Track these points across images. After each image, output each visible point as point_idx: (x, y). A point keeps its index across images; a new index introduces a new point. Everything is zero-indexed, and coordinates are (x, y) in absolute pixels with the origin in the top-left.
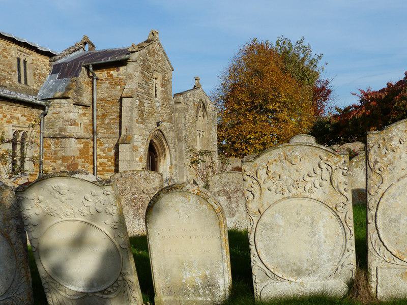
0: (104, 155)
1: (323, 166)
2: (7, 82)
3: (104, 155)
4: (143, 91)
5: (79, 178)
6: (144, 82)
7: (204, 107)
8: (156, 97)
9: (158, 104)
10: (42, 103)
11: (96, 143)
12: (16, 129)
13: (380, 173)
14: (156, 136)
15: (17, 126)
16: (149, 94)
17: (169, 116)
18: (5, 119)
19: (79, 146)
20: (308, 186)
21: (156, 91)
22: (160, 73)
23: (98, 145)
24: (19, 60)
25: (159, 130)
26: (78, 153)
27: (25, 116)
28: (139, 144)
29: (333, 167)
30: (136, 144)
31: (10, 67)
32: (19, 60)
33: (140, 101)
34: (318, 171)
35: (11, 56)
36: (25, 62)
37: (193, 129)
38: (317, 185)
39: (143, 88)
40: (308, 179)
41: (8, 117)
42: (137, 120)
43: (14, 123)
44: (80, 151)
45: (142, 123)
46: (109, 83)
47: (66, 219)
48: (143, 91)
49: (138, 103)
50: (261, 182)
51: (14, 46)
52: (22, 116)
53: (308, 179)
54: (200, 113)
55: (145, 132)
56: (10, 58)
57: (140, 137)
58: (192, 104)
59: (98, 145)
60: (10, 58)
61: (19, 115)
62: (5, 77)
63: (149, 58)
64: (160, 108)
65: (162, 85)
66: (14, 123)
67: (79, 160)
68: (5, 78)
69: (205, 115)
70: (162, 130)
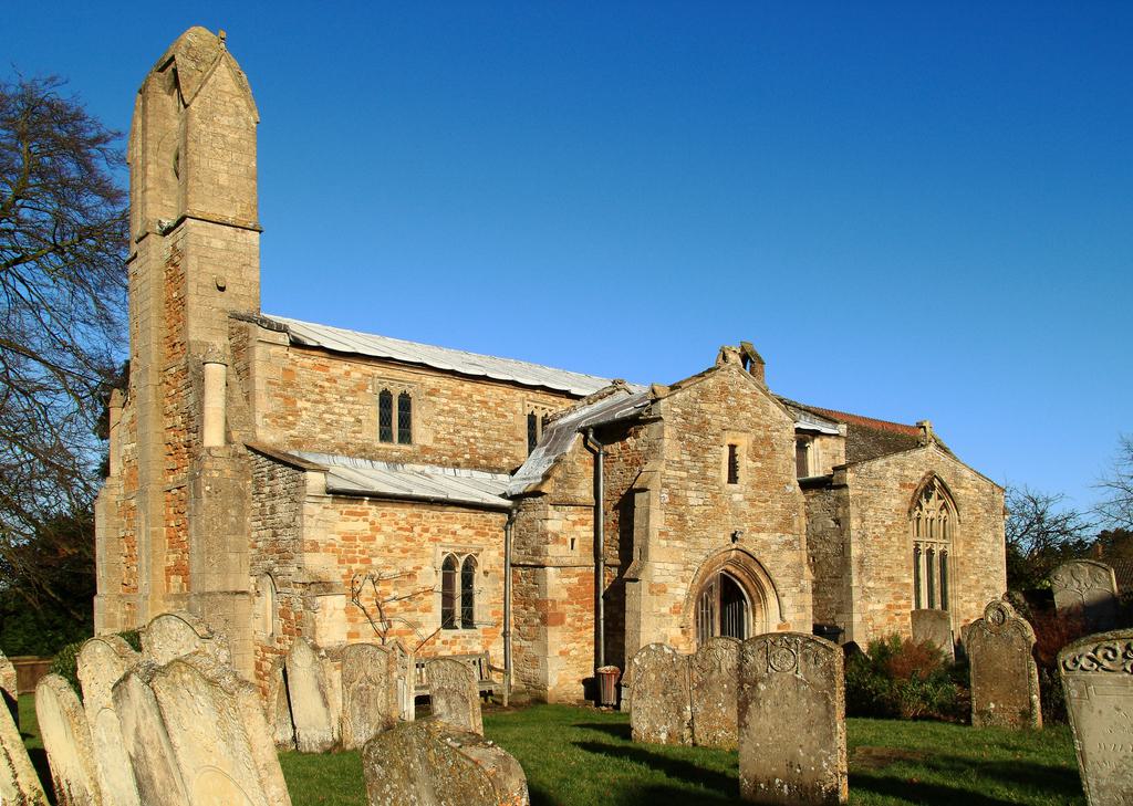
2: (505, 460)
4: (684, 474)
11: (605, 575)
12: (450, 551)
15: (451, 547)
19: (566, 581)
23: (607, 579)
26: (564, 595)
27: (472, 528)
30: (657, 580)
35: (515, 413)
43: (446, 540)
44: (569, 589)
48: (684, 474)
51: (520, 394)
52: (463, 528)
56: (510, 416)
59: (607, 579)
60: (510, 416)
61: (457, 527)
62: (500, 451)
63: (704, 406)
64: (745, 506)
66: (446, 540)
67: (568, 607)
68: (501, 453)
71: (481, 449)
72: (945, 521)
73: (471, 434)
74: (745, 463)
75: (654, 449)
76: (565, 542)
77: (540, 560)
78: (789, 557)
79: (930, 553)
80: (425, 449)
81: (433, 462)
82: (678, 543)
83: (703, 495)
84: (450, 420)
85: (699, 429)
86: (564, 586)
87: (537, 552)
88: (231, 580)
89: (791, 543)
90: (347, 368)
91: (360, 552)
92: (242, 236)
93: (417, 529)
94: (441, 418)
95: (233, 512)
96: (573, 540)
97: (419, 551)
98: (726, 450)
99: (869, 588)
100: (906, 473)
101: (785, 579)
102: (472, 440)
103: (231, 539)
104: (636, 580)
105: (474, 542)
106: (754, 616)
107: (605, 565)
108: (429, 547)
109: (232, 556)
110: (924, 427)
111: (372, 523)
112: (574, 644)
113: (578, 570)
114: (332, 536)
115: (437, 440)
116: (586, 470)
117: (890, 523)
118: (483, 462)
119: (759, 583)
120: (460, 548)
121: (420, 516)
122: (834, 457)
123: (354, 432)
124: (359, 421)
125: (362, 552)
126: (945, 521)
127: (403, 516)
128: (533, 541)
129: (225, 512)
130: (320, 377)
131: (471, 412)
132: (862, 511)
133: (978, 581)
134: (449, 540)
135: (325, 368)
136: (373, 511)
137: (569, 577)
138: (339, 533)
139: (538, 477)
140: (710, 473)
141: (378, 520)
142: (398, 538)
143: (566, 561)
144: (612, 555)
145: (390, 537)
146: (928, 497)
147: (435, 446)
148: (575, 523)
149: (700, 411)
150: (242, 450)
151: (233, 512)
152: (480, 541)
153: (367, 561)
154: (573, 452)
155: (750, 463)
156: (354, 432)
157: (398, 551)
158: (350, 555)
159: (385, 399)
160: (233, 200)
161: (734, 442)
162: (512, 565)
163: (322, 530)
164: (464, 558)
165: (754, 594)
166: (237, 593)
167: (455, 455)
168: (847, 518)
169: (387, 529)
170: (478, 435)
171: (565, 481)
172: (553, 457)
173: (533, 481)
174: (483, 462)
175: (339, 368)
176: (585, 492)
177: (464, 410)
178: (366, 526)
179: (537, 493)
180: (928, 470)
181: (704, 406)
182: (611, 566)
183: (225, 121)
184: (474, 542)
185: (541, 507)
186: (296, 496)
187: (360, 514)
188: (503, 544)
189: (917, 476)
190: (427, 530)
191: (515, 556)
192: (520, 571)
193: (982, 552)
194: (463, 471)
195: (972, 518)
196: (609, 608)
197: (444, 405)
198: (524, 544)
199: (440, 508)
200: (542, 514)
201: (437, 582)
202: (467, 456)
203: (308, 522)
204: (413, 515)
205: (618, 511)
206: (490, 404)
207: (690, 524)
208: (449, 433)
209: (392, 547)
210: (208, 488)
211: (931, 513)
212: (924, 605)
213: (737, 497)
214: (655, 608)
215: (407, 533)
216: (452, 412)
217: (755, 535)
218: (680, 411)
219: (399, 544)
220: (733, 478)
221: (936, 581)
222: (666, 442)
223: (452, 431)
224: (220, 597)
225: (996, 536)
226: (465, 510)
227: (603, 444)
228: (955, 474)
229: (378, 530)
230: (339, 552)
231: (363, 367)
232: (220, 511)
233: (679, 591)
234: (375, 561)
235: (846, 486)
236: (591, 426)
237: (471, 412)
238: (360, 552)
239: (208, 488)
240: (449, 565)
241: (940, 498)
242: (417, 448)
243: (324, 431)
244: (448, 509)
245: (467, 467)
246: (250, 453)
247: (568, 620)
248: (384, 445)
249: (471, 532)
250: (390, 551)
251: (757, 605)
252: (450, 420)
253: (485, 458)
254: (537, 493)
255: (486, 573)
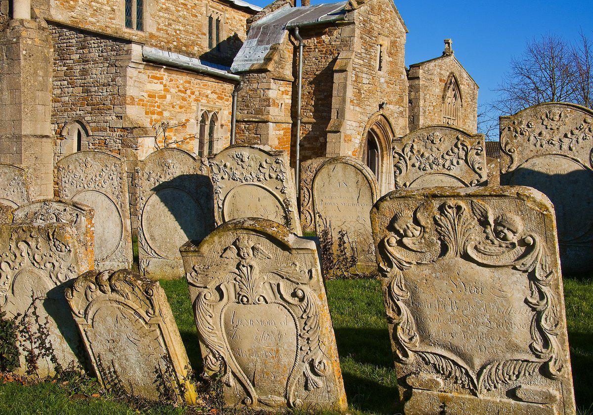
0: (308, 146)
1: (460, 146)
3: (308, 146)
4: (362, 62)
5: (257, 148)
6: (363, 51)
7: (457, 84)
8: (380, 69)
9: (382, 80)
10: (237, 77)
12: (205, 109)
13: (510, 153)
14: (378, 124)
16: (370, 66)
17: (397, 97)
18: (193, 97)
19: (278, 132)
20: (447, 164)
21: (380, 62)
22: (387, 37)
24: (211, 18)
25: (382, 115)
27: (216, 93)
28: (354, 132)
29: (469, 147)
30: (348, 132)
31: (200, 28)
32: (211, 18)
33: (357, 76)
34: (456, 150)
36: (218, 21)
37: (436, 115)
38: (455, 163)
39: (361, 58)
40: (447, 157)
41: (197, 93)
42: (352, 101)
44: (279, 139)
45: (358, 105)
46: (319, 51)
47: (246, 183)
48: (362, 62)
49: (354, 79)
50: (407, 159)
52: (212, 93)
53: (447, 157)
54: (450, 93)
55: (362, 117)
57: (354, 124)
58: (437, 79)
59: (301, 132)
63: (372, 17)
64: (385, 85)
65: (390, 54)
68: (194, 43)
69: (458, 95)
70: (387, 115)
73: (177, 27)
74: (386, 58)
75: (346, 44)
77: (264, 117)
80: (152, 36)
81: (156, 46)
82: (357, 108)
87: (259, 112)
88: (39, 126)
93: (188, 92)
94: (161, 14)
95: (40, 73)
96: (282, 104)
102: (178, 32)
103: (39, 94)
104: (339, 132)
105: (217, 103)
106: (382, 160)
107: (301, 123)
108: (194, 106)
109: (40, 108)
110: (449, 43)
111: (165, 86)
114: (143, 94)
115: (159, 30)
116: (289, 56)
118: (184, 48)
120: (210, 107)
121: (189, 82)
123: (110, 18)
124: (113, 10)
125: (159, 107)
127: (181, 82)
128: (256, 104)
129: (35, 73)
131: (178, 11)
134: (204, 101)
137: (279, 130)
138: (147, 92)
139: (260, 60)
141: (168, 84)
144: (307, 116)
147: (157, 34)
150: (44, 24)
151: (40, 73)
152: (219, 104)
153: (160, 113)
154: (283, 43)
156: (110, 18)
157: (177, 107)
158: (152, 108)
162: (237, 121)
163: (137, 89)
165: (384, 145)
166: (43, 137)
167: (168, 42)
168: (418, 99)
169: (173, 91)
171: (280, 63)
172: (269, 46)
173: (255, 62)
174: (184, 48)
176: (288, 72)
177: (174, 9)
178: (161, 87)
179: (262, 70)
180: (450, 71)
181: (372, 17)
182: (305, 123)
184: (217, 103)
185: (264, 80)
186: (117, 66)
188: (231, 106)
190: (193, 93)
191: (239, 115)
192: (243, 126)
194: (173, 54)
196: (303, 152)
198: (247, 106)
199: (201, 77)
200: (265, 86)
201: (196, 130)
202: (175, 43)
203: (130, 82)
205: (313, 86)
208: (165, 26)
209: (175, 104)
210: (24, 52)
215: (183, 95)
219: (178, 102)
222: (356, 39)
223: (167, 24)
224: (32, 139)
226: (214, 80)
227: (303, 39)
228: (460, 75)
230: (146, 105)
232: (32, 71)
234: (166, 114)
235: (418, 78)
236: (298, 26)
237: (178, 11)
239: (24, 52)
240: (204, 117)
243: (93, 15)
245: (175, 52)
246: (51, 27)
248: (128, 30)
249: (215, 96)
250: (173, 107)
251: (385, 152)
252: (166, 15)
253: (185, 46)
254: (262, 70)
255: (222, 126)
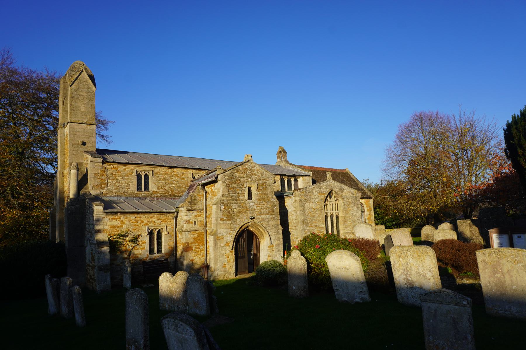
4: (230, 198)
56: (186, 179)
63: (238, 175)
64: (254, 207)
67: (193, 244)
71: (175, 190)
72: (337, 205)
73: (171, 186)
76: (192, 223)
78: (272, 222)
79: (332, 216)
82: (228, 222)
83: (237, 205)
84: (164, 182)
85: (235, 183)
86: (191, 238)
89: (274, 218)
90: (125, 168)
91: (117, 231)
92: (89, 127)
93: (139, 222)
94: (160, 181)
96: (195, 222)
97: (140, 229)
98: (247, 189)
99: (307, 230)
100: (321, 190)
101: (272, 230)
112: (196, 257)
113: (197, 232)
115: (158, 189)
117: (315, 207)
119: (261, 232)
122: (308, 183)
126: (337, 205)
130: (114, 171)
132: (304, 204)
133: (351, 224)
135: (116, 168)
136: (122, 217)
140: (240, 197)
141: (124, 220)
142: (131, 226)
143: (193, 229)
145: (129, 225)
146: (331, 197)
148: (196, 216)
149: (236, 176)
155: (256, 192)
156: (127, 189)
159: (139, 176)
160: (86, 115)
161: (250, 186)
164: (157, 230)
170: (174, 186)
175: (121, 168)
183: (83, 90)
187: (118, 219)
189: (326, 191)
193: (352, 214)
195: (348, 203)
197: (162, 177)
204: (138, 217)
206: (179, 175)
207: (232, 215)
208: (163, 186)
211: (332, 202)
212: (330, 232)
213: (251, 204)
214: (219, 244)
215: (136, 224)
216: (165, 179)
217: (259, 216)
218: (228, 177)
220: (250, 197)
221: (335, 225)
225: (358, 208)
229: (124, 223)
231: (131, 167)
233: (228, 238)
238: (117, 231)
241: (335, 197)
242: (151, 192)
243: (115, 189)
244: (151, 214)
247: (194, 249)
248: (138, 192)
249: (160, 221)
252: (164, 182)
